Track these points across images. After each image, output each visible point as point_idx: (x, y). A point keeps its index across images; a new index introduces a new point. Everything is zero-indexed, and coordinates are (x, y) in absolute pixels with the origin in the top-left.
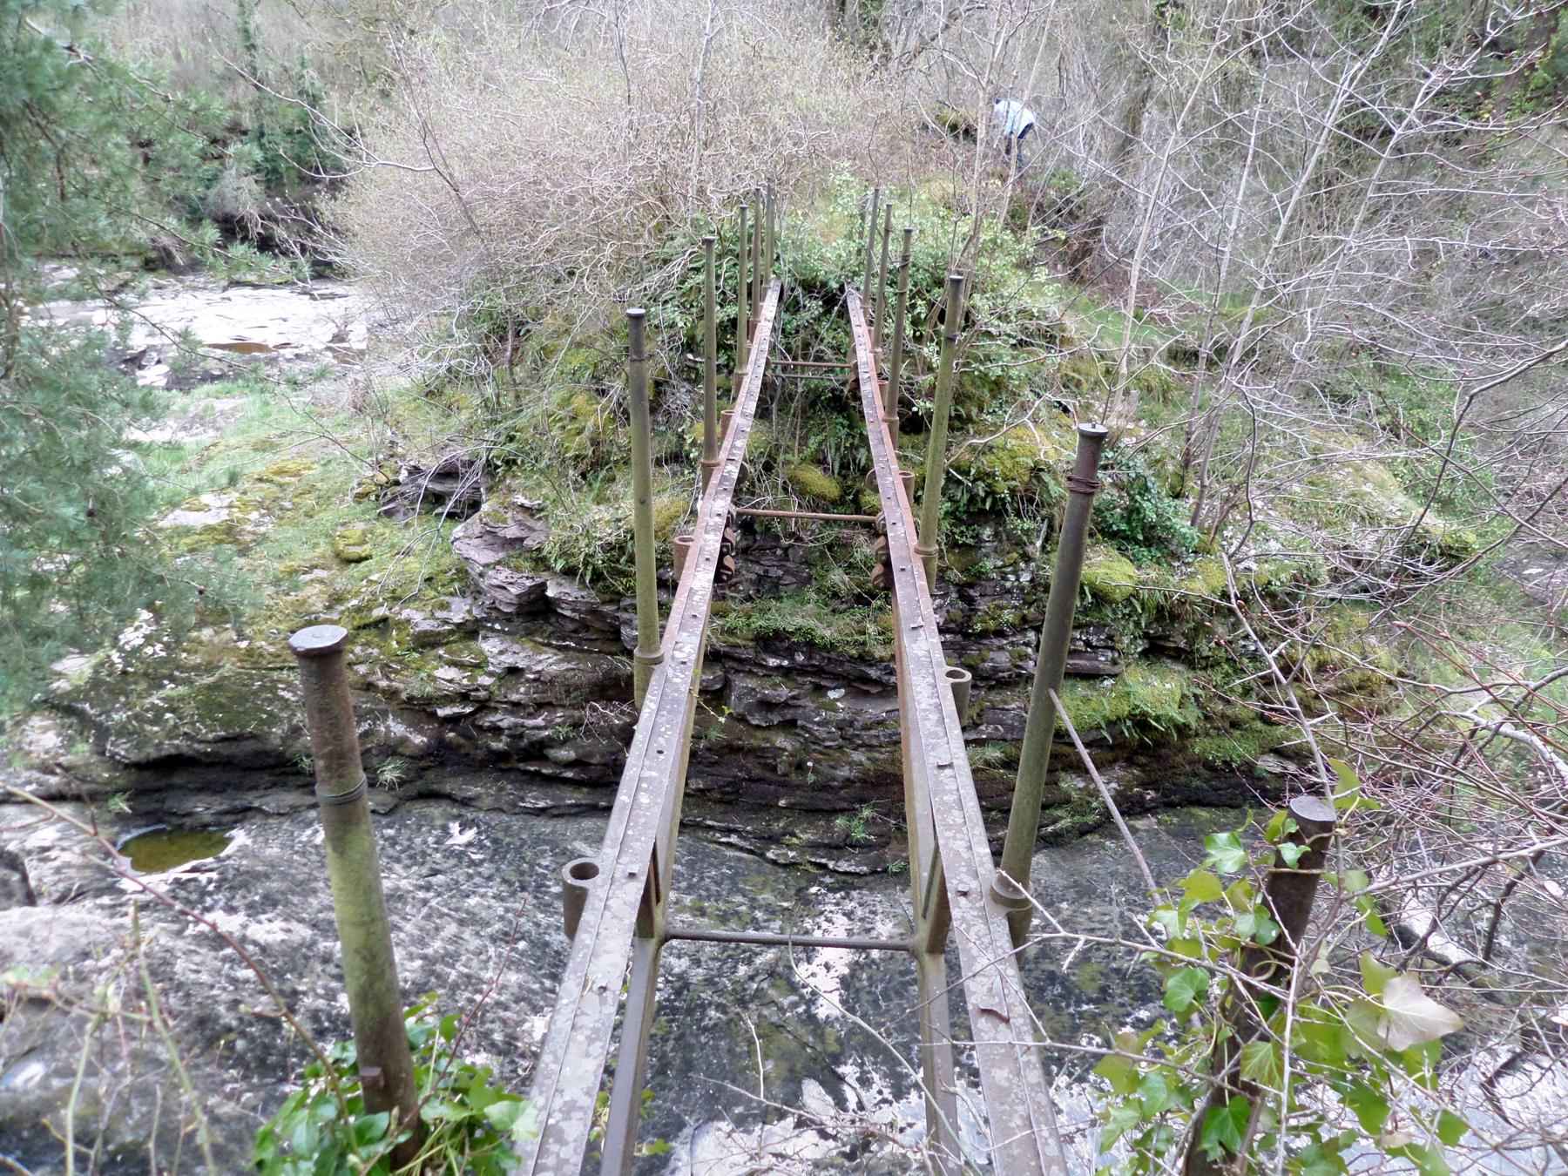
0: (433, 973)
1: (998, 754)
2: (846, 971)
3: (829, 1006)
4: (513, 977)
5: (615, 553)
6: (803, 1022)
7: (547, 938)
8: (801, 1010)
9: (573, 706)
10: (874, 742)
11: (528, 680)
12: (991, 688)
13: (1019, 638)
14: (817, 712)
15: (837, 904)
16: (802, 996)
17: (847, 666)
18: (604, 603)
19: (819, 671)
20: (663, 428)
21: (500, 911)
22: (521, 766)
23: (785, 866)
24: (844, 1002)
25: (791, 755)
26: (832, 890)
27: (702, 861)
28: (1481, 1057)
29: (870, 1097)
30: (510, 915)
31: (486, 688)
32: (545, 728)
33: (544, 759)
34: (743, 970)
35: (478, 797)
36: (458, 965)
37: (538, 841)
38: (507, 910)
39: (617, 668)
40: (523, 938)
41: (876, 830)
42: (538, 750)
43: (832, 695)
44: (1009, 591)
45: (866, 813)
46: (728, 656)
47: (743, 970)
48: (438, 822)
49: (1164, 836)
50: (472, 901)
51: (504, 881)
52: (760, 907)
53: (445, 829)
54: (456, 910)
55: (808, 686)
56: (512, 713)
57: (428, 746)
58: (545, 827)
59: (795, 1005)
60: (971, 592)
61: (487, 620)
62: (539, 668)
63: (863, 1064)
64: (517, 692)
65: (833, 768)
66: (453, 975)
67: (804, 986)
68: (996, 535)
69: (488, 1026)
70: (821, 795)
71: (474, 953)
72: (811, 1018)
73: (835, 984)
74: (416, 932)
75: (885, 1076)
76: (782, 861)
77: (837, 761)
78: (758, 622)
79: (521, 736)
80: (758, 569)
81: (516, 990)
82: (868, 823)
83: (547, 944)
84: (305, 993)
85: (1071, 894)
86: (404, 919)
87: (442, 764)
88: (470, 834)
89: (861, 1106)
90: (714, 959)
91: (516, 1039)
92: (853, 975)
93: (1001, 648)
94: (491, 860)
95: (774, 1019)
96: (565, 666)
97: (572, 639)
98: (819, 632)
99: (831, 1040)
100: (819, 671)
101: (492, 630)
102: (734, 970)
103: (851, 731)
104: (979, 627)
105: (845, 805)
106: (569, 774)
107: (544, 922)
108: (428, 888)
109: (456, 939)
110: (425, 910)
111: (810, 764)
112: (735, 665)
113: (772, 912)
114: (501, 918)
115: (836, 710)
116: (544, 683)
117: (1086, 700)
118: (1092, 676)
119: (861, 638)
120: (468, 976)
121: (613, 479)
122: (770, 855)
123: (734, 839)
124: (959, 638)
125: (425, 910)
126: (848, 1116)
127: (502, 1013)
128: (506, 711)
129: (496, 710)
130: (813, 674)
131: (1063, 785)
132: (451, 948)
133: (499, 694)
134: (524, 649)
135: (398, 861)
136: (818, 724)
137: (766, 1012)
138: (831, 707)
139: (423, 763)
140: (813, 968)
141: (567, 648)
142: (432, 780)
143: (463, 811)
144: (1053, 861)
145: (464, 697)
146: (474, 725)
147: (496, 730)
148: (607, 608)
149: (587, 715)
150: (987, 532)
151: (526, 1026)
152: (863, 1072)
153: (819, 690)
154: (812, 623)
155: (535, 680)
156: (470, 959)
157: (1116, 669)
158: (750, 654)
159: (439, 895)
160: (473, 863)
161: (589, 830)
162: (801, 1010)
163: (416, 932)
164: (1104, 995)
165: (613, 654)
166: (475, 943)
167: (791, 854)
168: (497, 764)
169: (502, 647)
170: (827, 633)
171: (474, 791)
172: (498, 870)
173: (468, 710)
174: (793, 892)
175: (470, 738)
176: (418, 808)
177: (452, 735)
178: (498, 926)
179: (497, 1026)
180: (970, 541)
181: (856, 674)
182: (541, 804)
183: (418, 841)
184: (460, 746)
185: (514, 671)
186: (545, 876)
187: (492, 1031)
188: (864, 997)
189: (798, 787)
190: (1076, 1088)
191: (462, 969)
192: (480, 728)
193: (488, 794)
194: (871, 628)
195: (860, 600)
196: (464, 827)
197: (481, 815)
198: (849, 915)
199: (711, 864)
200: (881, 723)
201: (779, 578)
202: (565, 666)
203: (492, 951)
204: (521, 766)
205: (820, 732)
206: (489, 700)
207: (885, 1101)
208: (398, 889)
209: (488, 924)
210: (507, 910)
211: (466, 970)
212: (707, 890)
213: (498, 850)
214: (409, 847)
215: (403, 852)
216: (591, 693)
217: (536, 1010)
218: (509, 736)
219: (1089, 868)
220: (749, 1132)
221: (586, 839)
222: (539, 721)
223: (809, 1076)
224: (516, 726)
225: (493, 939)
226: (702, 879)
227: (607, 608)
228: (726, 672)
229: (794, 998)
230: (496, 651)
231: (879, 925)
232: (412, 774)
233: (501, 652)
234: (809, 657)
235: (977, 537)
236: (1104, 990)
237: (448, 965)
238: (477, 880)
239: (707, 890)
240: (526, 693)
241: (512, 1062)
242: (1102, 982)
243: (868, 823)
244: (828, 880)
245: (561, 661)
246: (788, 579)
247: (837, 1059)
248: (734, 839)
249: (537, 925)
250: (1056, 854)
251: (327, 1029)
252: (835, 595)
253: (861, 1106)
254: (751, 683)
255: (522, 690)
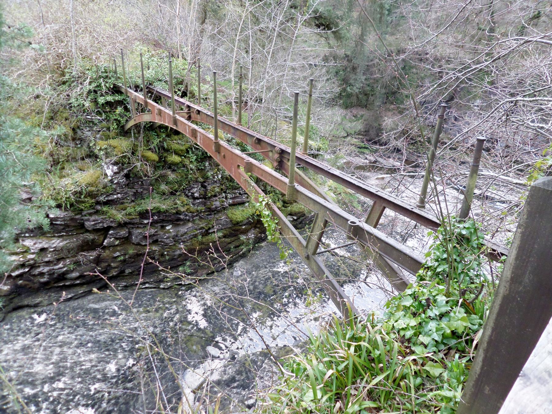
0: (60, 367)
1: (221, 234)
2: (203, 312)
3: (203, 324)
4: (93, 356)
5: (78, 195)
6: (197, 331)
7: (98, 339)
8: (195, 328)
9: (72, 257)
10: (185, 240)
11: (50, 252)
12: (215, 214)
13: (221, 196)
14: (164, 234)
15: (190, 294)
16: (193, 324)
17: (173, 217)
18: (76, 215)
19: (163, 221)
20: (79, 146)
21: (74, 337)
22: (56, 285)
23: (168, 289)
24: (207, 321)
25: (159, 252)
26: (187, 291)
27: (139, 296)
28: (362, 276)
29: (228, 343)
30: (79, 337)
31: (33, 259)
32: (64, 267)
33: (66, 279)
34: (171, 324)
35: (41, 302)
36: (68, 361)
37: (74, 310)
38: (76, 336)
39: (86, 238)
40: (88, 343)
41: (193, 268)
42: (62, 277)
43: (168, 228)
44: (216, 182)
45: (188, 263)
46: (130, 223)
47: (171, 324)
48: (27, 317)
49: (270, 246)
50: (60, 338)
51: (69, 327)
52: (166, 303)
53: (32, 318)
54: (56, 343)
55: (159, 227)
56: (47, 266)
57: (11, 289)
58: (75, 304)
59: (193, 328)
60: (205, 184)
61: (21, 233)
62: (54, 245)
63: (221, 336)
64: (47, 257)
65: (174, 252)
66: (69, 365)
67: (193, 321)
68: (210, 164)
69: (93, 374)
70: (173, 262)
71: (72, 354)
72: (200, 329)
73: (201, 317)
74: (44, 356)
75: (229, 336)
76: (166, 287)
77: (175, 249)
78: (139, 209)
79: (54, 273)
80: (134, 190)
81: (96, 359)
82: (190, 266)
83: (99, 341)
84: (8, 395)
85: (254, 269)
86: (35, 354)
87: (19, 295)
88: (44, 316)
89: (227, 347)
90: (160, 324)
91: (107, 374)
92: (205, 313)
93: (216, 200)
94: (59, 322)
95: (189, 334)
96: (65, 242)
97: (63, 232)
98: (161, 208)
99: (209, 333)
100: (163, 221)
101: (25, 237)
102: (169, 325)
103: (177, 238)
104: (209, 195)
105: (181, 263)
106: (78, 282)
107: (93, 334)
108: (38, 340)
109: (62, 353)
110: (42, 348)
111: (166, 253)
112: (132, 226)
113: (171, 303)
114: (76, 339)
115: (170, 233)
116: (57, 251)
117: (243, 211)
118: (243, 203)
119: (176, 206)
120: (75, 362)
121: (63, 168)
122: (162, 287)
123: (147, 285)
124: (204, 200)
125: (42, 348)
126: (225, 351)
127: (96, 369)
128: (44, 266)
129: (39, 266)
130: (160, 222)
131: (241, 239)
132: (61, 356)
133: (39, 260)
134: (43, 241)
135: (18, 335)
136: (166, 239)
137: (185, 333)
138: (168, 232)
139: (11, 297)
140: (192, 315)
141: (62, 236)
142: (17, 302)
143: (36, 309)
144: (245, 262)
145: (23, 266)
146: (30, 275)
147: (42, 274)
148: (77, 217)
149: (80, 258)
150: (207, 164)
151: (107, 369)
152: (223, 338)
153: (163, 227)
154: (158, 205)
155: (54, 251)
156: (71, 357)
157: (248, 200)
158: (137, 221)
159: (44, 341)
160: (51, 326)
161: (92, 299)
162: (195, 328)
163: (44, 356)
164: (275, 293)
165: (82, 233)
166: (70, 351)
167: (169, 284)
168: (46, 287)
169: (34, 242)
170: (164, 207)
171: (38, 300)
172: (64, 324)
173: (27, 270)
174: (174, 296)
175: (30, 281)
176: (14, 314)
177: (21, 282)
178: (76, 342)
179: (97, 373)
180: (203, 168)
181: (175, 219)
182: (69, 296)
183: (22, 326)
184: (26, 285)
185: (43, 250)
186: (84, 320)
187: (96, 376)
188: (212, 318)
189: (164, 262)
190: (280, 319)
191: (71, 361)
192: (34, 276)
193: (45, 300)
194: (178, 202)
195: (172, 194)
196: (39, 314)
197: (45, 308)
198: (195, 296)
199: (143, 296)
200: (186, 233)
201: (142, 192)
202: (65, 242)
203: (79, 351)
204: (56, 285)
205: (167, 241)
206: (35, 263)
207: (233, 343)
208: (25, 345)
209: (71, 343)
210: (76, 336)
211: (73, 361)
212: (146, 304)
213: (60, 318)
214: (20, 329)
215: (18, 331)
216: (78, 250)
217: (108, 363)
218: (48, 275)
219: (255, 261)
220: (199, 368)
221: (93, 303)
222: (61, 265)
223: (208, 345)
224: (50, 270)
225: (77, 347)
226: (142, 302)
227: (77, 217)
228: (129, 229)
229: (191, 326)
230: (32, 244)
231: (205, 296)
232: (8, 302)
233: (35, 244)
234: (159, 217)
235: (204, 166)
236: (274, 291)
237: (64, 362)
238: (57, 330)
239: (146, 304)
240: (52, 257)
241: (109, 382)
242: (273, 290)
243: (190, 266)
244: (183, 288)
245: (61, 242)
246: (145, 192)
247: (214, 337)
248: (147, 285)
249: (92, 336)
250: (245, 259)
251: (197, 328)
252: (164, 194)
253: (227, 347)
254: (140, 231)
255: (49, 256)
